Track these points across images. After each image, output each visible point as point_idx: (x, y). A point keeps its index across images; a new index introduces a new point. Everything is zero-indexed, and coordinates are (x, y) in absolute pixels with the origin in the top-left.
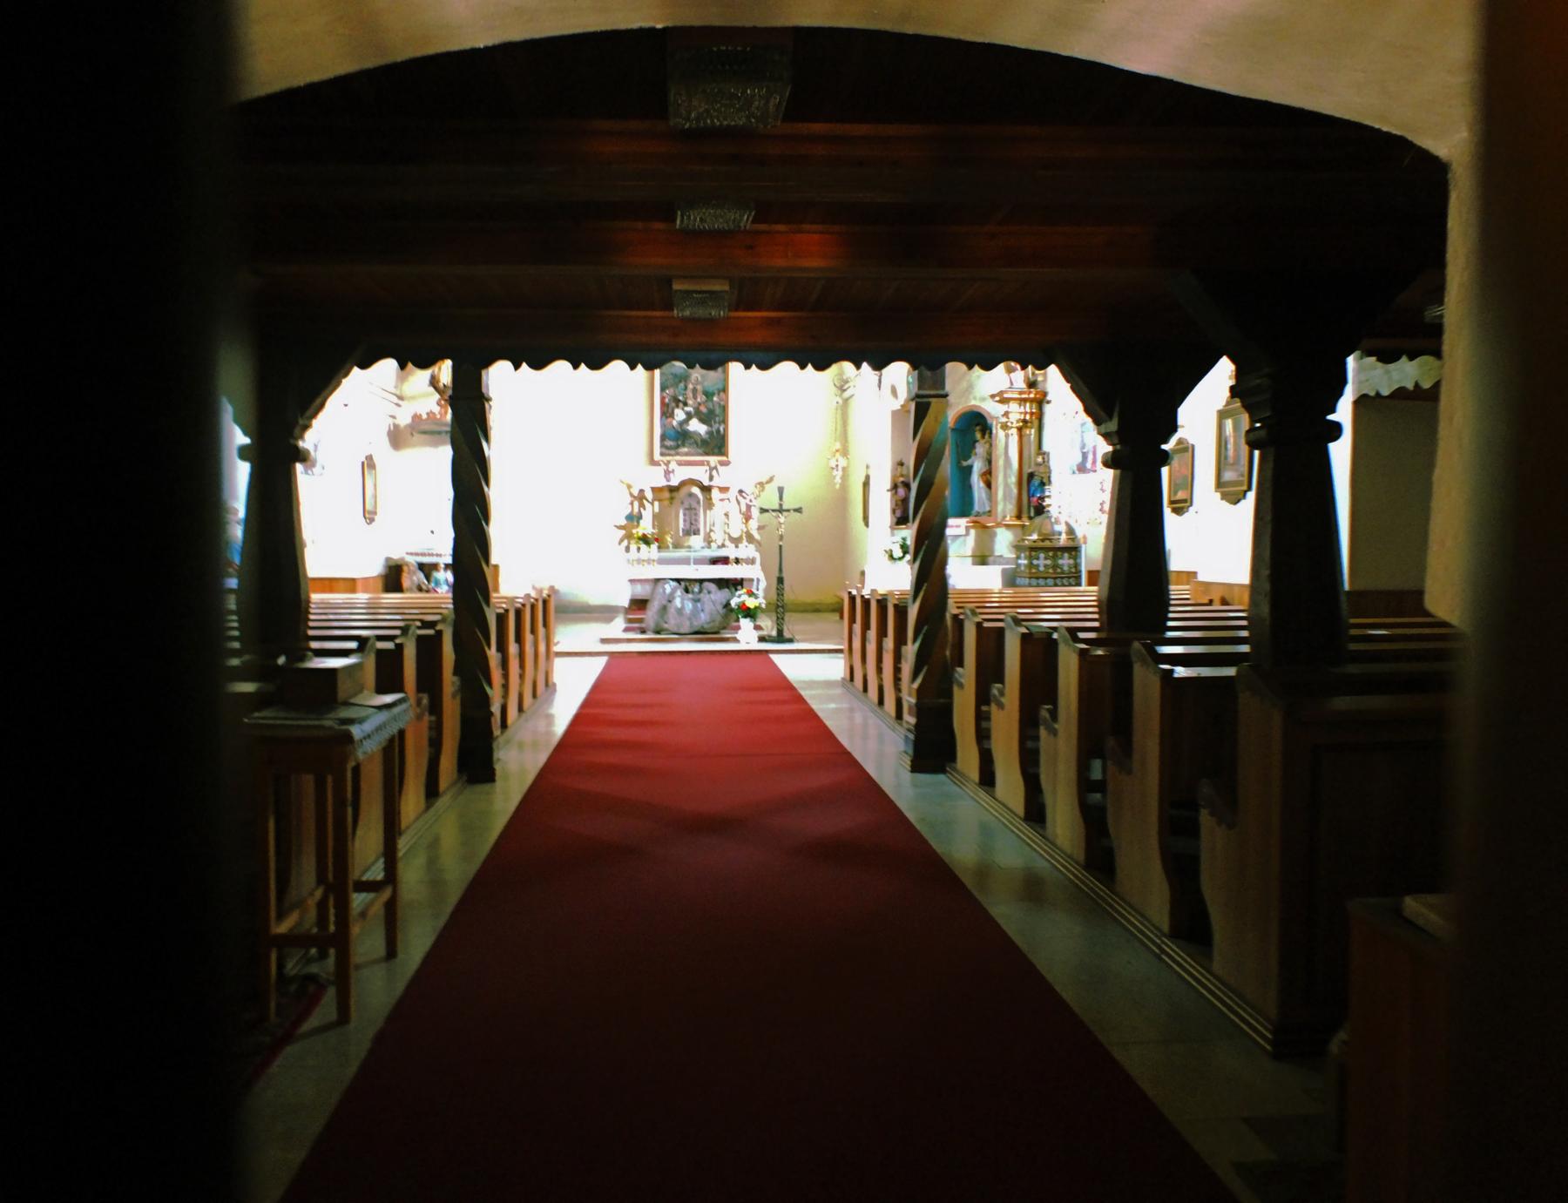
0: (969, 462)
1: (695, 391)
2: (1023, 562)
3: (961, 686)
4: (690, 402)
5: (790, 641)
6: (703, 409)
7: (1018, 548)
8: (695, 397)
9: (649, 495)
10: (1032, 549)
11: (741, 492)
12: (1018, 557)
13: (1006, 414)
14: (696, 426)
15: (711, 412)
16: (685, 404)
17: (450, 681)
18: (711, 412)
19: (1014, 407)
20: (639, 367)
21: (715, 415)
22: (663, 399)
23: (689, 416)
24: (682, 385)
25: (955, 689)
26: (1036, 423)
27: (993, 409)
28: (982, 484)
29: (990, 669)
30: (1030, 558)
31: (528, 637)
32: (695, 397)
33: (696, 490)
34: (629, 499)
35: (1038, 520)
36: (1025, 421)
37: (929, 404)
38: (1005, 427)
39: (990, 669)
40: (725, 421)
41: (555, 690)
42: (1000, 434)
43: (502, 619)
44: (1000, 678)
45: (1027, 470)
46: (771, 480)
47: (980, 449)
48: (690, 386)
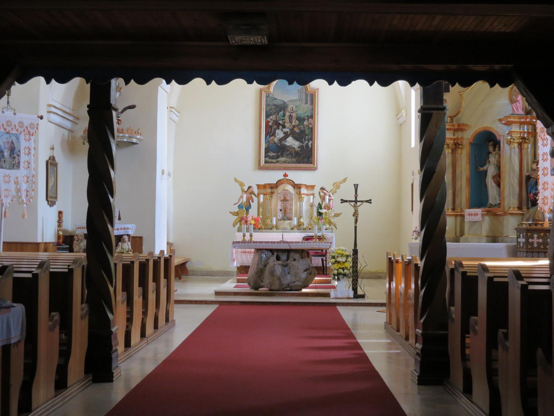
0: (485, 168)
1: (291, 117)
2: (522, 240)
3: (453, 320)
4: (287, 125)
5: (363, 296)
6: (297, 130)
7: (519, 230)
8: (291, 122)
9: (256, 191)
10: (528, 231)
11: (322, 189)
12: (518, 237)
13: (510, 133)
14: (291, 142)
15: (302, 132)
16: (284, 127)
17: (79, 309)
18: (302, 132)
19: (515, 128)
20: (213, 82)
21: (305, 132)
22: (267, 123)
23: (286, 135)
24: (281, 113)
25: (450, 322)
26: (532, 139)
27: (501, 130)
28: (494, 185)
29: (469, 307)
30: (527, 238)
31: (151, 285)
32: (291, 122)
33: (290, 188)
34: (240, 193)
35: (532, 210)
36: (523, 138)
37: (431, 115)
38: (509, 143)
39: (469, 307)
40: (312, 139)
41: (174, 324)
42: (505, 148)
43: (128, 269)
44: (505, 324)
45: (525, 173)
46: (345, 180)
47: (493, 159)
48: (288, 114)
